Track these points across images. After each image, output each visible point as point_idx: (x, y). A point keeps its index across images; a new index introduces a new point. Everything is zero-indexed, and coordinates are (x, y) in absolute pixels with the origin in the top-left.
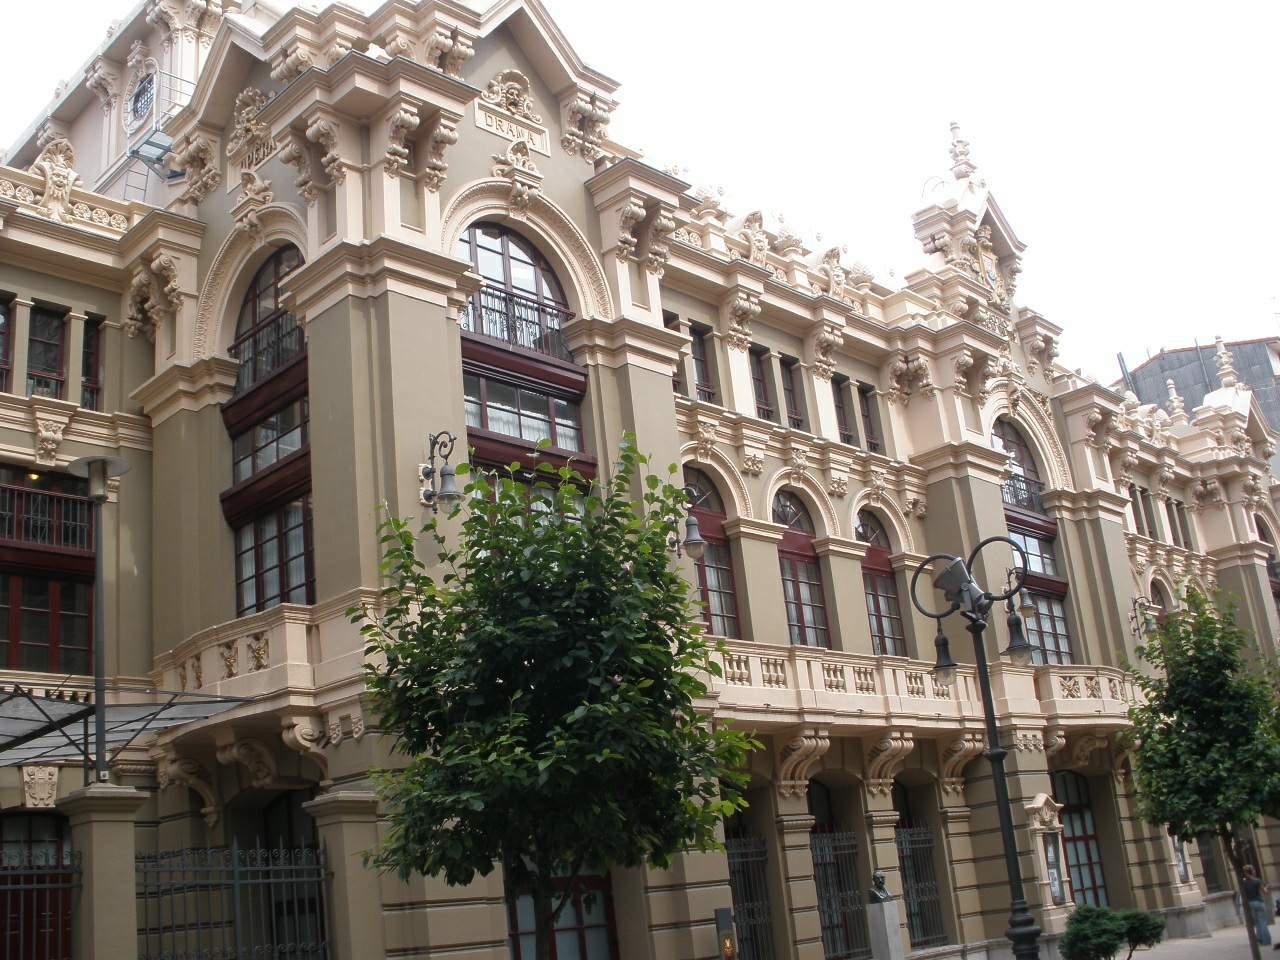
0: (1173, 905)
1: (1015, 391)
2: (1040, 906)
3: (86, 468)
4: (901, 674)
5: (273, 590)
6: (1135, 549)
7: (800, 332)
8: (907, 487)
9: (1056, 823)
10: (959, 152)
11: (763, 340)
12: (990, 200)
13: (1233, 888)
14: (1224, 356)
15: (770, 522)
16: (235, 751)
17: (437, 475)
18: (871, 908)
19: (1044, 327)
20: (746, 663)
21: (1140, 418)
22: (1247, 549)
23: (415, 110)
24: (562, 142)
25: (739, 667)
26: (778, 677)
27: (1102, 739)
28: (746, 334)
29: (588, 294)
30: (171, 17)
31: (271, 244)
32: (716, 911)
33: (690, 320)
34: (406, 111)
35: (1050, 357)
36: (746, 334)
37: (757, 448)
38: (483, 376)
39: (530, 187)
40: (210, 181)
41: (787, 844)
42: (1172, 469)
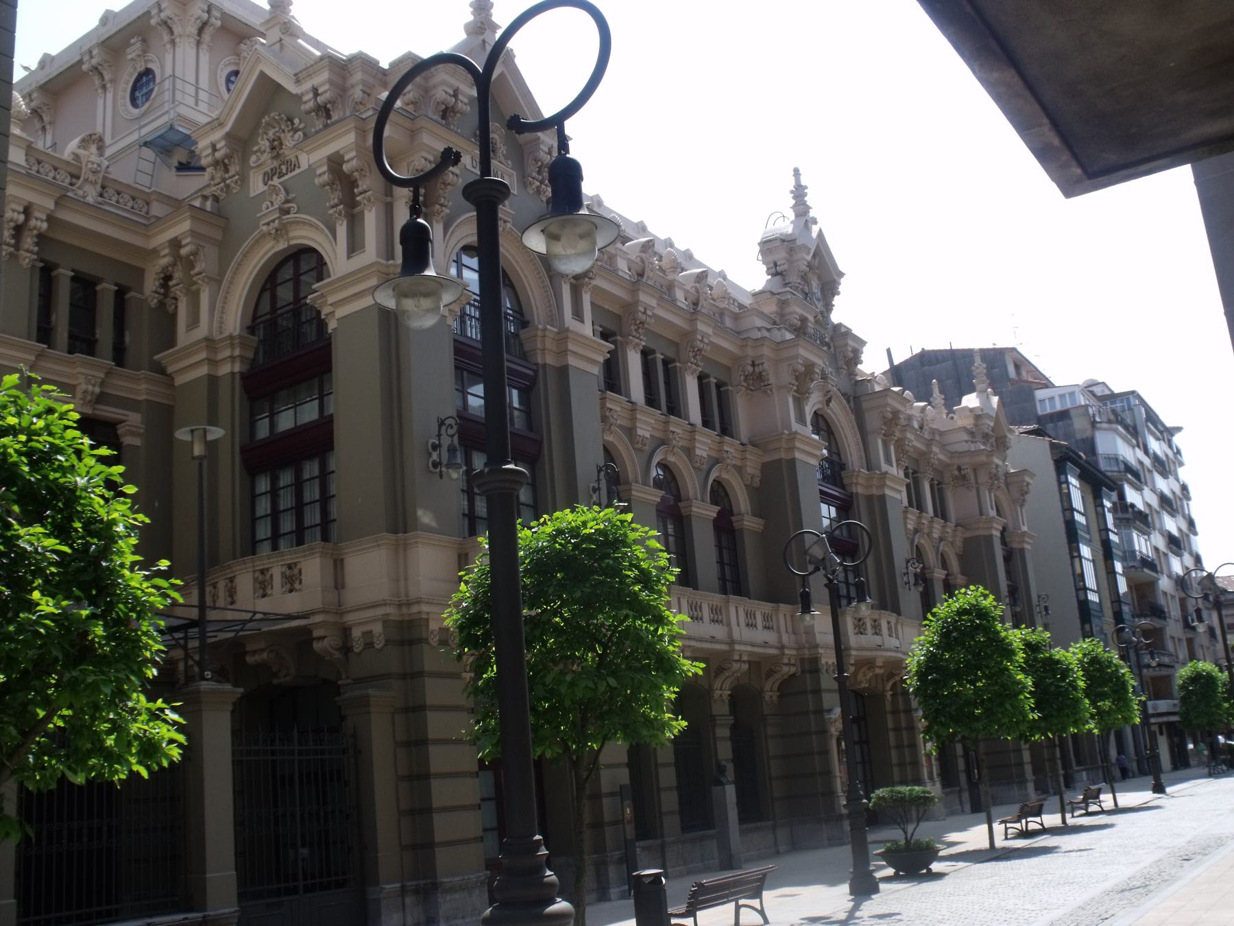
3: (190, 434)
4: (741, 610)
5: (287, 524)
10: (799, 193)
14: (979, 366)
16: (265, 655)
21: (915, 413)
27: (881, 667)
30: (175, 23)
31: (290, 247)
38: (466, 370)
40: (233, 185)
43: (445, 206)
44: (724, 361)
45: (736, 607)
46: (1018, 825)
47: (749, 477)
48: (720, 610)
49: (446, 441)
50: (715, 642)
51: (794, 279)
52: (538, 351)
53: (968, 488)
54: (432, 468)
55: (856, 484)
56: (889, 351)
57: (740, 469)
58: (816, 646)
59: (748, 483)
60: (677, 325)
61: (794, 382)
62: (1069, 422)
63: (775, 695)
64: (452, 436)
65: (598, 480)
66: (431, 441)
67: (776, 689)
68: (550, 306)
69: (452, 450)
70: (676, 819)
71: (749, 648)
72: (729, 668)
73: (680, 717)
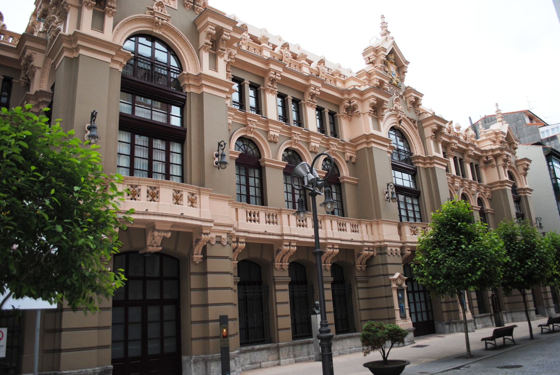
0: (59, 370)
1: (400, 117)
2: (395, 318)
6: (454, 181)
7: (302, 90)
8: (347, 151)
9: (404, 285)
10: (384, 26)
11: (322, 105)
12: (394, 43)
13: (491, 312)
15: (321, 170)
17: (220, 156)
19: (415, 93)
20: (345, 225)
22: (502, 182)
23: (214, 28)
24: (184, 4)
25: (343, 226)
26: (269, 220)
28: (314, 102)
29: (190, 62)
32: (220, 316)
33: (249, 82)
34: (211, 29)
35: (418, 105)
36: (314, 102)
37: (315, 143)
39: (162, 20)
41: (276, 289)
42: (472, 151)
45: (331, 221)
46: (548, 327)
49: (390, 190)
53: (492, 167)
56: (470, 118)
62: (557, 140)
64: (392, 189)
66: (215, 153)
68: (196, 64)
69: (392, 193)
70: (289, 334)
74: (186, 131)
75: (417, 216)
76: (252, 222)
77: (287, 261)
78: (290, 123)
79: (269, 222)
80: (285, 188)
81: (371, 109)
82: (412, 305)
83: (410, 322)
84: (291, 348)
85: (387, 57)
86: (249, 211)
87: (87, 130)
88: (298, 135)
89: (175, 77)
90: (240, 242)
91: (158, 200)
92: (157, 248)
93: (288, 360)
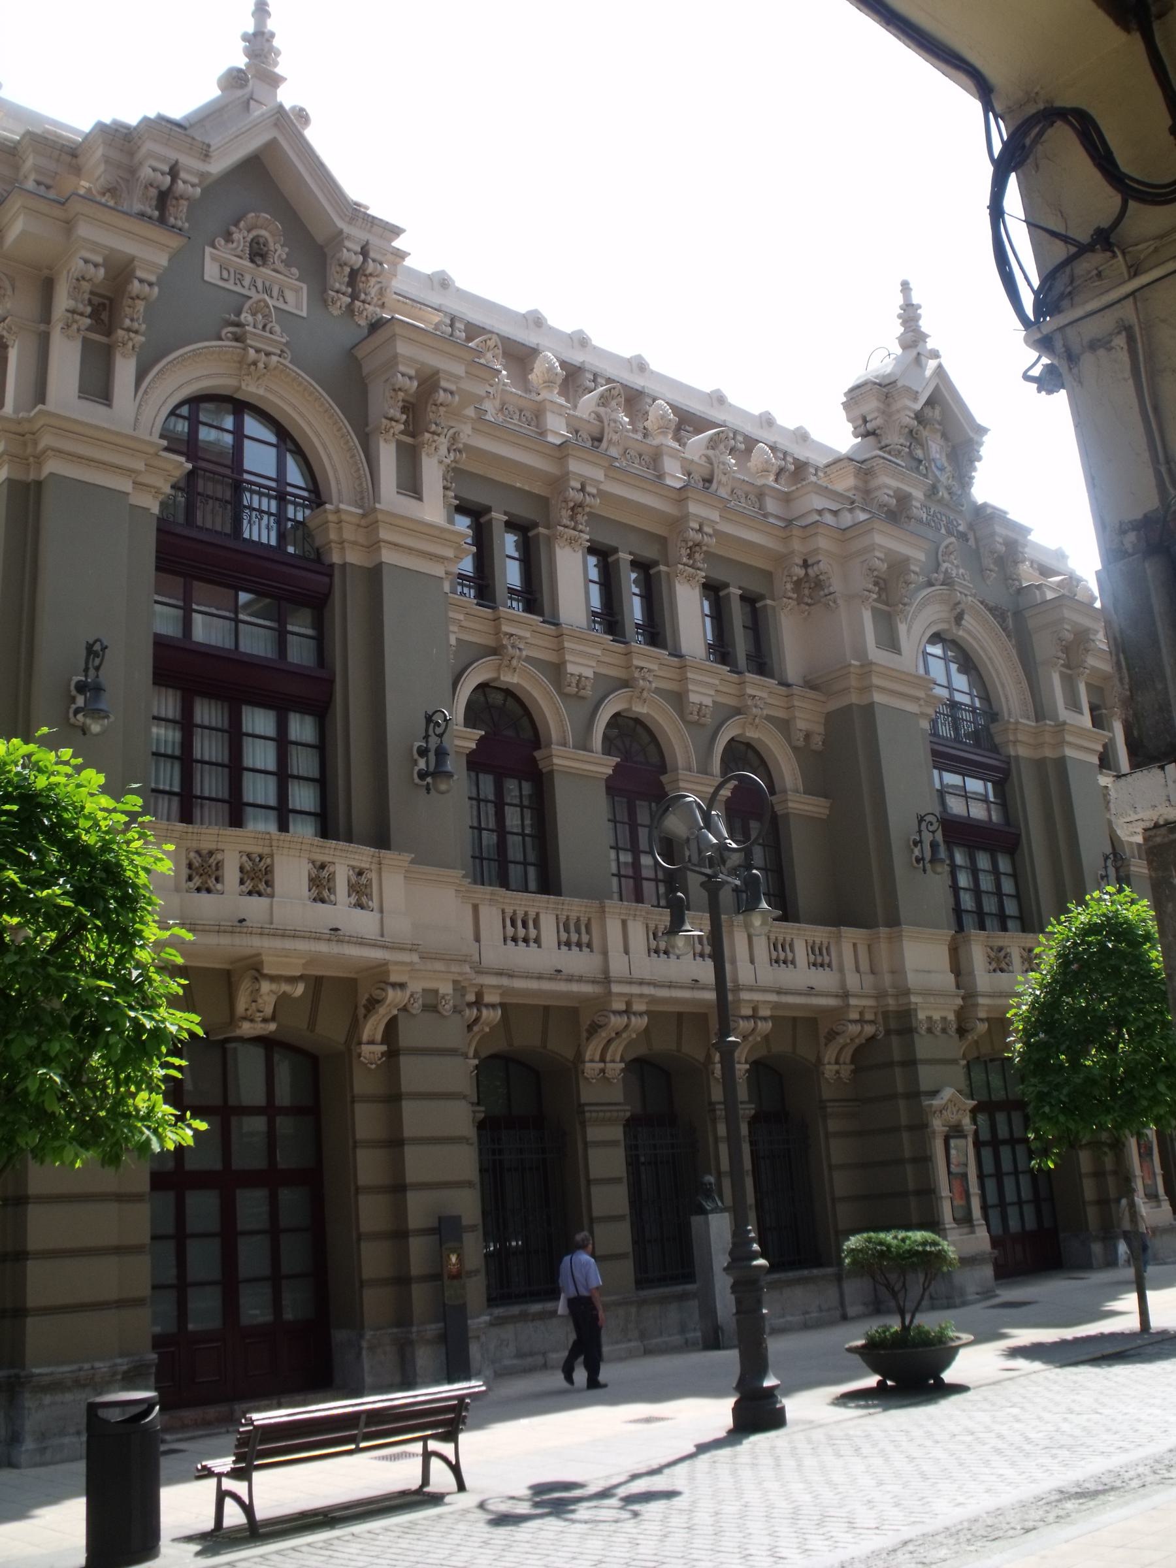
10: (910, 315)
17: (432, 756)
18: (696, 1220)
26: (569, 939)
33: (506, 513)
43: (439, 435)
44: (537, 489)
47: (801, 735)
48: (828, 949)
49: (927, 838)
50: (698, 989)
51: (895, 439)
52: (333, 545)
54: (417, 780)
55: (1015, 742)
57: (784, 726)
58: (907, 992)
59: (801, 743)
60: (535, 469)
61: (1060, 654)
63: (846, 1071)
64: (933, 832)
65: (1106, 867)
67: (848, 1060)
69: (934, 846)
71: (773, 998)
72: (605, 1025)
73: (188, 1114)
74: (331, 682)
75: (1011, 908)
76: (521, 943)
77: (618, 1058)
78: (624, 636)
79: (568, 944)
80: (611, 834)
81: (871, 586)
82: (991, 1184)
83: (982, 1233)
84: (633, 1310)
85: (919, 417)
86: (509, 911)
87: (74, 692)
88: (647, 658)
89: (300, 517)
90: (487, 1006)
91: (269, 890)
92: (262, 1025)
93: (623, 1346)
